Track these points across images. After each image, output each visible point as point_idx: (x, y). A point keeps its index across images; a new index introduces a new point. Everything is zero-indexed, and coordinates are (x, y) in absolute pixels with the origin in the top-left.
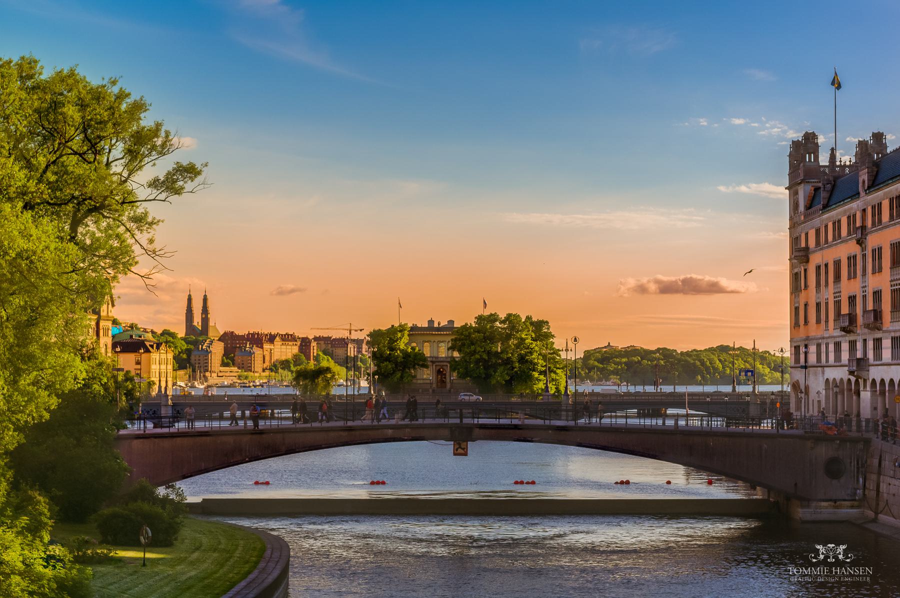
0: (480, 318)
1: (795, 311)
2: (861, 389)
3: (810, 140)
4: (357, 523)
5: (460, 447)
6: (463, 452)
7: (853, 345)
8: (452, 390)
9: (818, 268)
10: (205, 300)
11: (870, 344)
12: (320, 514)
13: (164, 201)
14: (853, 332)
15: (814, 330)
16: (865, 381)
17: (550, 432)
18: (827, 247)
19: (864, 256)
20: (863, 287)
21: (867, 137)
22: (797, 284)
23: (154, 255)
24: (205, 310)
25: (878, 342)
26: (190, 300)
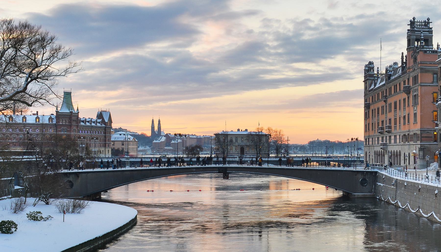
0: (258, 129)
1: (366, 126)
2: (385, 154)
6: (227, 177)
7: (383, 138)
9: (373, 110)
10: (159, 121)
11: (388, 138)
12: (106, 200)
13: (64, 76)
14: (383, 134)
15: (371, 133)
16: (386, 151)
17: (257, 169)
18: (375, 103)
19: (386, 106)
20: (386, 117)
22: (366, 116)
23: (60, 97)
25: (390, 137)
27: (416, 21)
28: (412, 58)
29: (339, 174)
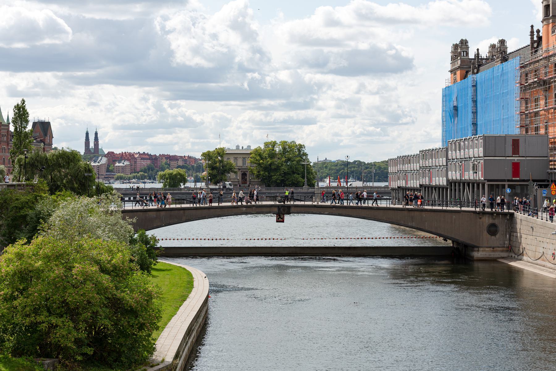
0: (266, 144)
3: (464, 43)
4: (347, 267)
5: (280, 217)
6: (281, 220)
8: (250, 185)
10: (96, 134)
21: (495, 41)
24: (96, 139)
26: (87, 134)
28: (553, 34)
29: (454, 216)
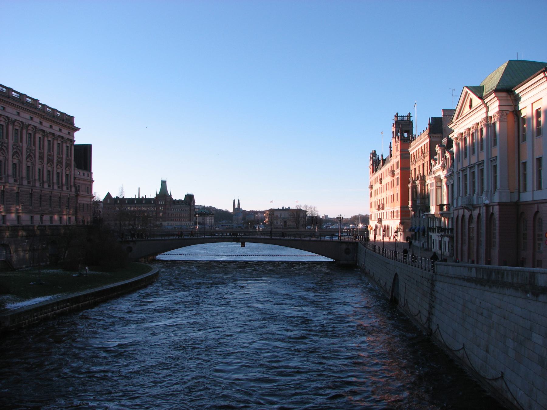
10: (239, 201)
26: (234, 201)
27: (399, 115)
